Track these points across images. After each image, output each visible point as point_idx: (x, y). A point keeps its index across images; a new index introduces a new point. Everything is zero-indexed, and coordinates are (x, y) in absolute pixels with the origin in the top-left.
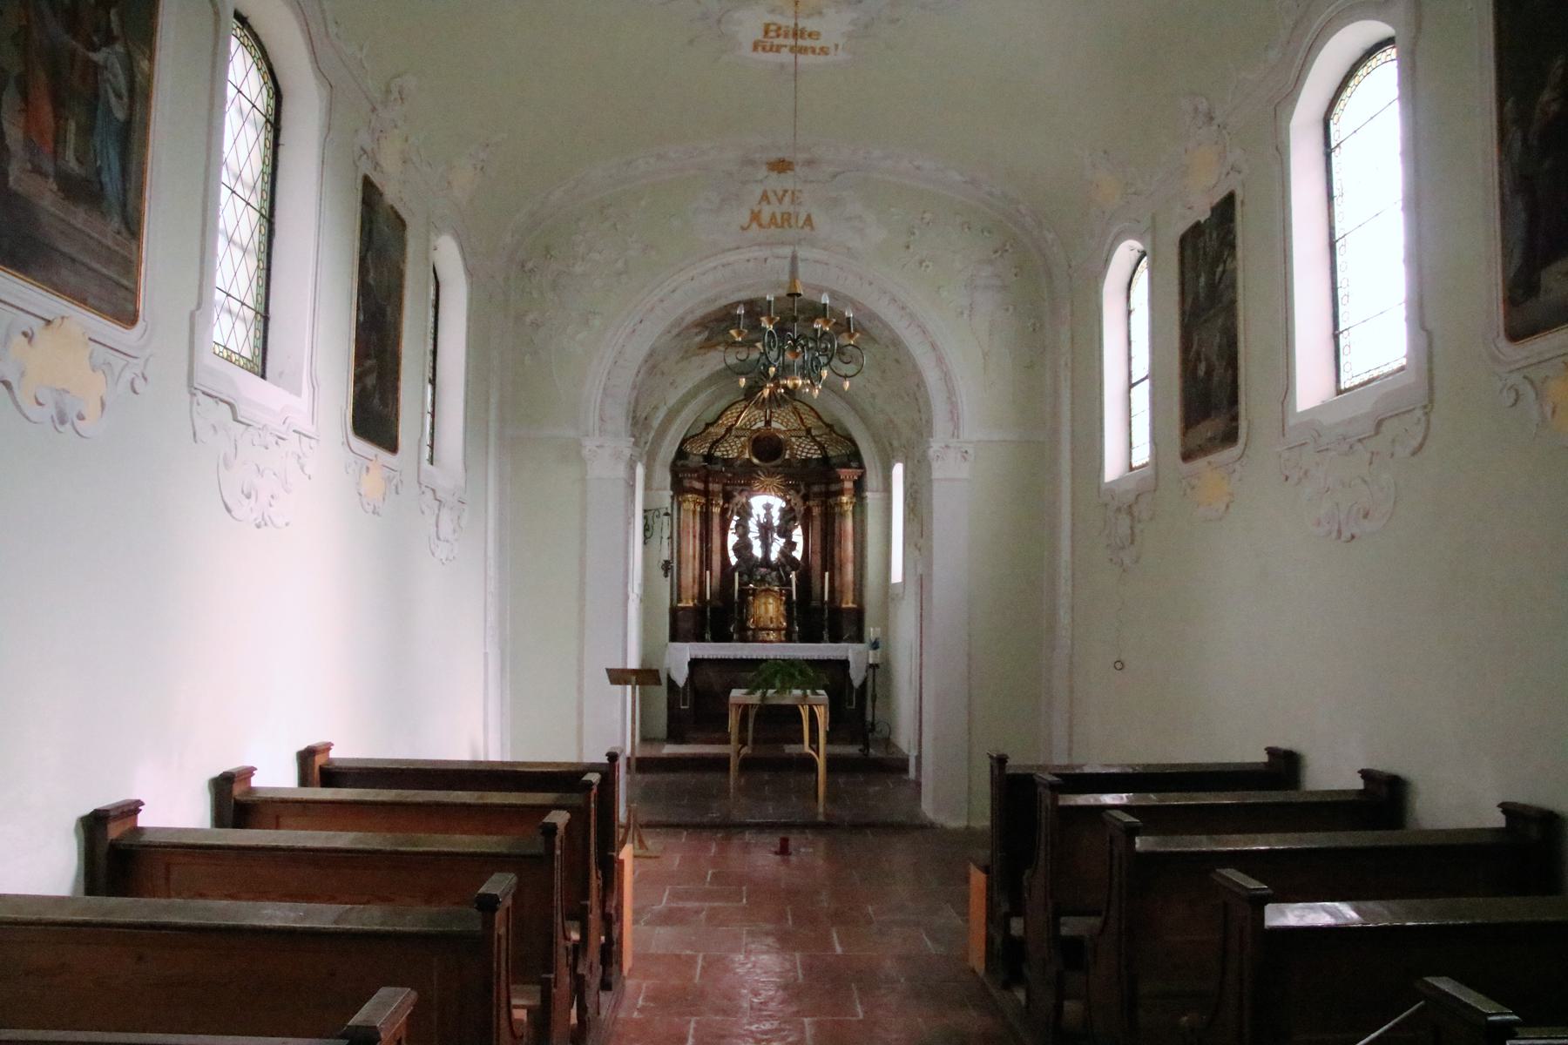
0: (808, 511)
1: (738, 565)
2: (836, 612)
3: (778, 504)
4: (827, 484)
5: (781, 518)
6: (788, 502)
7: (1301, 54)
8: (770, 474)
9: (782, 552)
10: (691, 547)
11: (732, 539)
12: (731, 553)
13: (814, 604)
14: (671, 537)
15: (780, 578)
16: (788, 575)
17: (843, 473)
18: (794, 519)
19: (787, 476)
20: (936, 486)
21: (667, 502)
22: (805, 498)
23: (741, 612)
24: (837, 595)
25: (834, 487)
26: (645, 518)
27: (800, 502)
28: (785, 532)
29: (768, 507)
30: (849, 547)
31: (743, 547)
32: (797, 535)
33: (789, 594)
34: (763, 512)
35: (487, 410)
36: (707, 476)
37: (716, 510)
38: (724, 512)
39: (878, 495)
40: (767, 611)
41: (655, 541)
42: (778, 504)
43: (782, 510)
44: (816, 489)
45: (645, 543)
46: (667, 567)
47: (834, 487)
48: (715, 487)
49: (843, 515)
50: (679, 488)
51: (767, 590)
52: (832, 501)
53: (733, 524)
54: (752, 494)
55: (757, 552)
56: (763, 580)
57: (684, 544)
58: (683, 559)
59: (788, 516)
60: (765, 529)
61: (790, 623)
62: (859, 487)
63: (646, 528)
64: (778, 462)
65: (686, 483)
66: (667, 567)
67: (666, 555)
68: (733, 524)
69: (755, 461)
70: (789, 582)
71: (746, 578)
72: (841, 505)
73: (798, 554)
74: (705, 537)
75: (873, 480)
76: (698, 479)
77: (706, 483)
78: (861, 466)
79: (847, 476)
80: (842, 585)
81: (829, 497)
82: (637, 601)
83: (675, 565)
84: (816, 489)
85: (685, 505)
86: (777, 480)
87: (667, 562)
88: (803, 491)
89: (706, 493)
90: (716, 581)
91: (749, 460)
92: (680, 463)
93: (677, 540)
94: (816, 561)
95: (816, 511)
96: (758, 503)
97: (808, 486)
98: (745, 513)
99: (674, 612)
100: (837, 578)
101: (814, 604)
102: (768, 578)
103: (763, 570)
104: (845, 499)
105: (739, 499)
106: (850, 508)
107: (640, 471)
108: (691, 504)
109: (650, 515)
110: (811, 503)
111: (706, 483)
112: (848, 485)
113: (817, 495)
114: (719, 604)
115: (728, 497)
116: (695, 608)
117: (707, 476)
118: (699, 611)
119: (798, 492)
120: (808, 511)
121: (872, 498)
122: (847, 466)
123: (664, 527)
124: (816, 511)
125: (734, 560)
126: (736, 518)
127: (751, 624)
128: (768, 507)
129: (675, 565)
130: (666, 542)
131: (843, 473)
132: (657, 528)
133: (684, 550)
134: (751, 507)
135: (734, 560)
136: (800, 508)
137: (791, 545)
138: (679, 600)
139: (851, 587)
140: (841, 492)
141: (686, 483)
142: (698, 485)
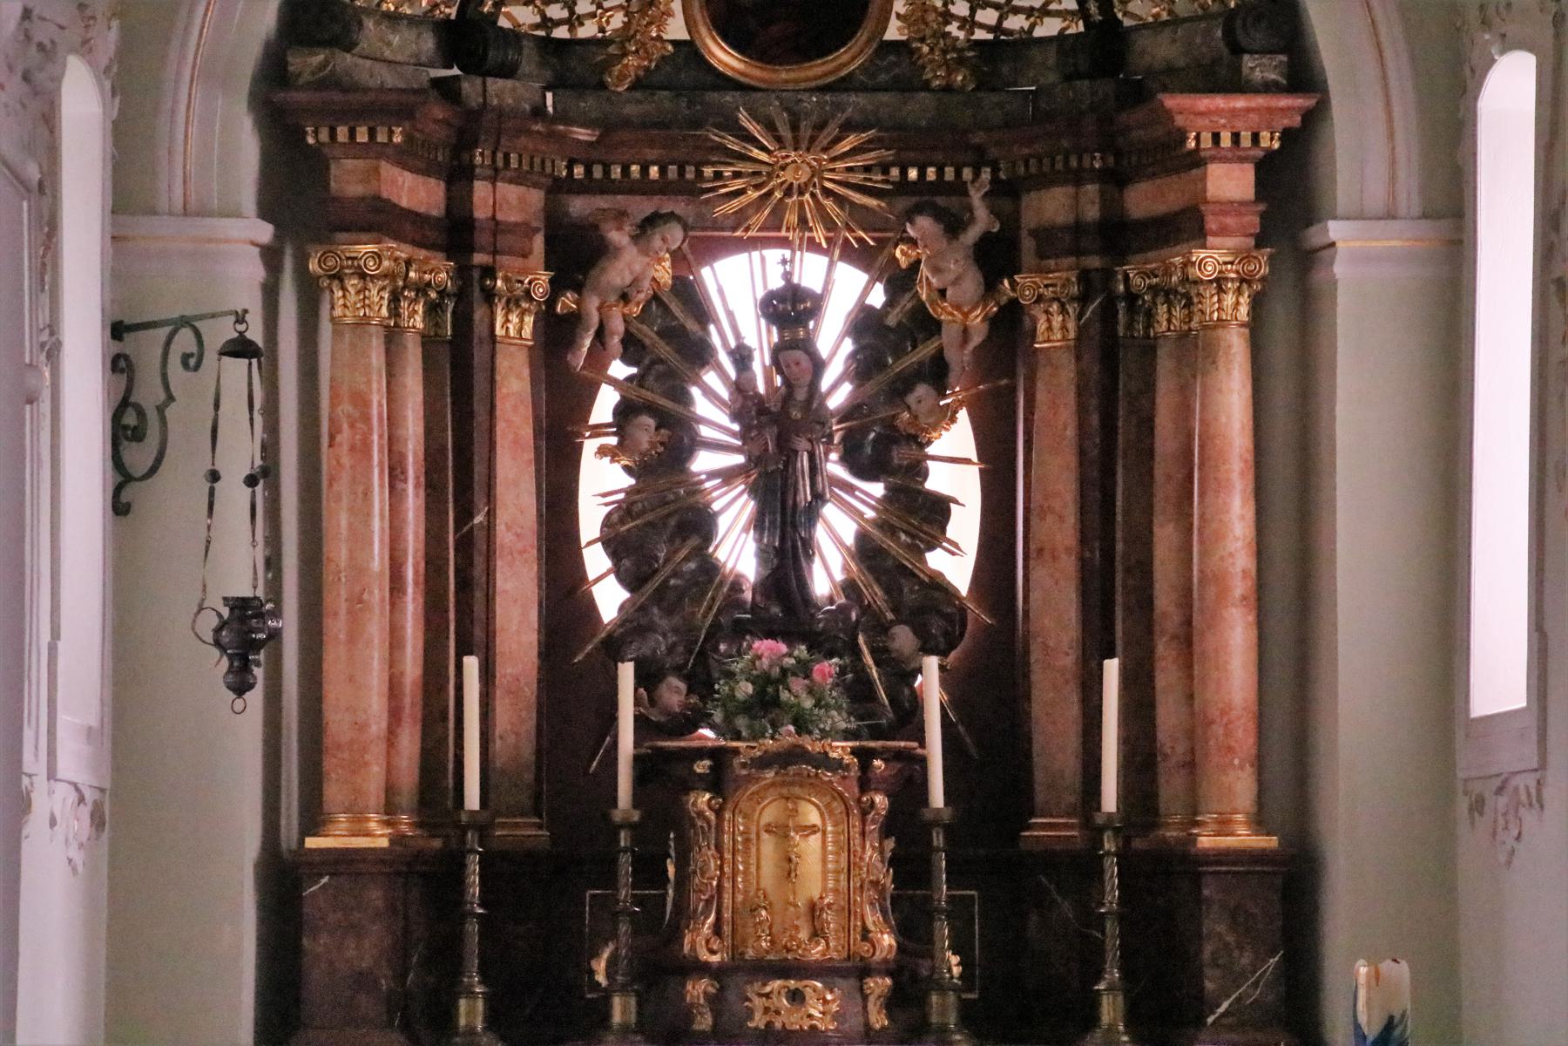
0: (1009, 325)
1: (633, 623)
2: (1166, 878)
3: (845, 289)
4: (1116, 180)
5: (864, 368)
6: (900, 282)
7: (46, 423)
8: (800, 130)
9: (867, 552)
10: (379, 526)
11: (601, 481)
12: (596, 560)
13: (1049, 828)
14: (265, 475)
15: (858, 691)
16: (902, 675)
17: (1202, 115)
18: (937, 373)
19: (905, 141)
20: (746, 255)
21: (242, 280)
22: (995, 258)
23: (649, 871)
24: (1170, 788)
25: (1143, 200)
26: (119, 365)
27: (971, 284)
28: (887, 449)
29: (790, 310)
30: (1234, 517)
31: (662, 526)
32: (953, 464)
33: (911, 785)
34: (759, 337)
35: (332, 379)
36: (464, 140)
37: (515, 328)
38: (556, 333)
39: (1394, 239)
40: (789, 867)
41: (174, 494)
42: (845, 289)
43: (865, 324)
44: (1051, 206)
45: (119, 507)
46: (244, 634)
47: (1143, 200)
48: (504, 201)
49: (1196, 349)
50: (300, 201)
51: (791, 757)
52: (1134, 274)
53: (605, 404)
54: (711, 247)
55: (738, 551)
56: (766, 702)
57: (338, 520)
58: (337, 599)
59: (897, 347)
60: (779, 429)
61: (911, 921)
62: (1290, 185)
63: (127, 426)
64: (848, 58)
65: (348, 179)
66: (244, 634)
67: (240, 576)
68: (605, 404)
69: (723, 57)
70: (909, 717)
71: (674, 693)
72: (1185, 294)
73: (955, 564)
74: (457, 473)
75: (1364, 152)
76: (405, 157)
77: (458, 176)
78: (1302, 76)
79: (1224, 132)
80: (1196, 728)
81: (1121, 253)
82: (77, 824)
83: (289, 624)
84: (1051, 206)
85: (342, 303)
86: (843, 161)
87: (242, 608)
88: (982, 220)
89: (455, 233)
90: (517, 718)
91: (688, 50)
92: (306, 63)
93: (298, 493)
94: (1053, 602)
95: (1053, 330)
96: (737, 285)
97: (1006, 192)
98: (672, 338)
99: (284, 881)
100: (1166, 677)
101: (1049, 828)
102: (796, 693)
103: (768, 650)
104: (1210, 258)
105: (639, 266)
106: (1235, 305)
107: (82, 102)
108: (375, 290)
109: (146, 348)
110: (1025, 285)
111: (458, 176)
112: (1230, 182)
113: (1050, 242)
114: (528, 832)
115: (576, 254)
116: (398, 866)
117: (464, 140)
118: (423, 877)
119: (953, 225)
120: (1009, 325)
121: (1361, 251)
122: (1220, 77)
123: (224, 417)
124: (1053, 330)
125: (610, 598)
126: (619, 370)
127: (701, 943)
128: (790, 310)
129: (289, 624)
130: (235, 497)
131: (1202, 115)
132: (187, 420)
133: (338, 552)
134: (701, 312)
135: (610, 598)
136: (965, 318)
137: (925, 514)
138: (314, 819)
139: (1244, 737)
140: (1187, 225)
141: (348, 179)
142: (417, 192)
